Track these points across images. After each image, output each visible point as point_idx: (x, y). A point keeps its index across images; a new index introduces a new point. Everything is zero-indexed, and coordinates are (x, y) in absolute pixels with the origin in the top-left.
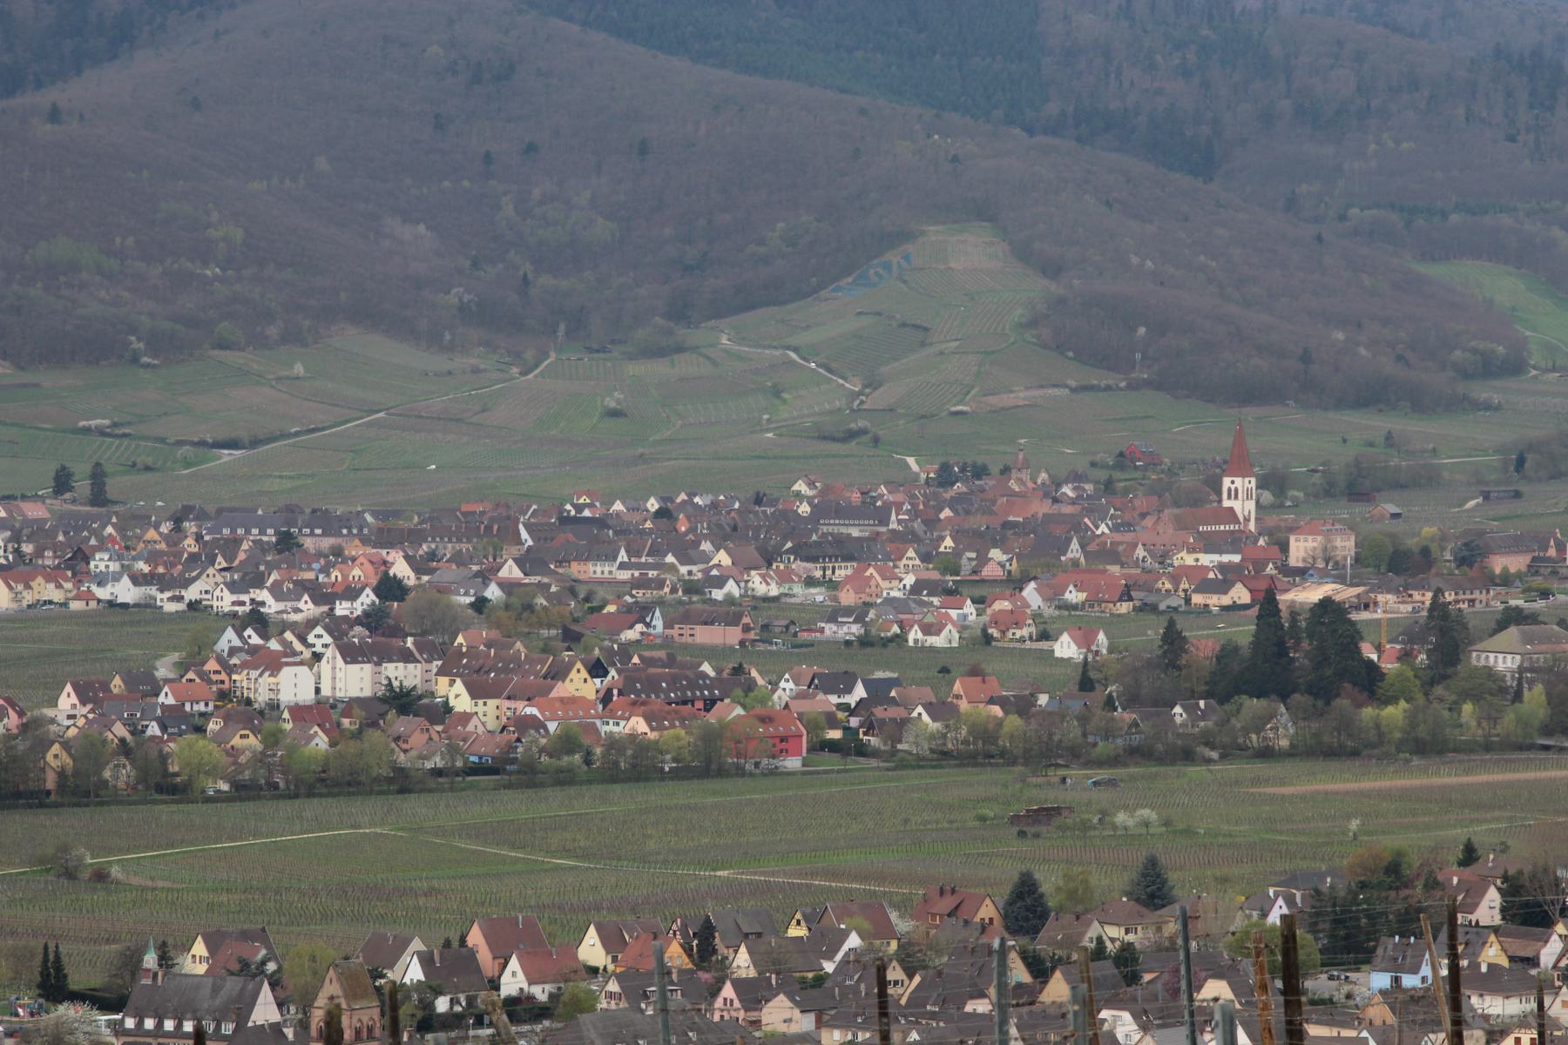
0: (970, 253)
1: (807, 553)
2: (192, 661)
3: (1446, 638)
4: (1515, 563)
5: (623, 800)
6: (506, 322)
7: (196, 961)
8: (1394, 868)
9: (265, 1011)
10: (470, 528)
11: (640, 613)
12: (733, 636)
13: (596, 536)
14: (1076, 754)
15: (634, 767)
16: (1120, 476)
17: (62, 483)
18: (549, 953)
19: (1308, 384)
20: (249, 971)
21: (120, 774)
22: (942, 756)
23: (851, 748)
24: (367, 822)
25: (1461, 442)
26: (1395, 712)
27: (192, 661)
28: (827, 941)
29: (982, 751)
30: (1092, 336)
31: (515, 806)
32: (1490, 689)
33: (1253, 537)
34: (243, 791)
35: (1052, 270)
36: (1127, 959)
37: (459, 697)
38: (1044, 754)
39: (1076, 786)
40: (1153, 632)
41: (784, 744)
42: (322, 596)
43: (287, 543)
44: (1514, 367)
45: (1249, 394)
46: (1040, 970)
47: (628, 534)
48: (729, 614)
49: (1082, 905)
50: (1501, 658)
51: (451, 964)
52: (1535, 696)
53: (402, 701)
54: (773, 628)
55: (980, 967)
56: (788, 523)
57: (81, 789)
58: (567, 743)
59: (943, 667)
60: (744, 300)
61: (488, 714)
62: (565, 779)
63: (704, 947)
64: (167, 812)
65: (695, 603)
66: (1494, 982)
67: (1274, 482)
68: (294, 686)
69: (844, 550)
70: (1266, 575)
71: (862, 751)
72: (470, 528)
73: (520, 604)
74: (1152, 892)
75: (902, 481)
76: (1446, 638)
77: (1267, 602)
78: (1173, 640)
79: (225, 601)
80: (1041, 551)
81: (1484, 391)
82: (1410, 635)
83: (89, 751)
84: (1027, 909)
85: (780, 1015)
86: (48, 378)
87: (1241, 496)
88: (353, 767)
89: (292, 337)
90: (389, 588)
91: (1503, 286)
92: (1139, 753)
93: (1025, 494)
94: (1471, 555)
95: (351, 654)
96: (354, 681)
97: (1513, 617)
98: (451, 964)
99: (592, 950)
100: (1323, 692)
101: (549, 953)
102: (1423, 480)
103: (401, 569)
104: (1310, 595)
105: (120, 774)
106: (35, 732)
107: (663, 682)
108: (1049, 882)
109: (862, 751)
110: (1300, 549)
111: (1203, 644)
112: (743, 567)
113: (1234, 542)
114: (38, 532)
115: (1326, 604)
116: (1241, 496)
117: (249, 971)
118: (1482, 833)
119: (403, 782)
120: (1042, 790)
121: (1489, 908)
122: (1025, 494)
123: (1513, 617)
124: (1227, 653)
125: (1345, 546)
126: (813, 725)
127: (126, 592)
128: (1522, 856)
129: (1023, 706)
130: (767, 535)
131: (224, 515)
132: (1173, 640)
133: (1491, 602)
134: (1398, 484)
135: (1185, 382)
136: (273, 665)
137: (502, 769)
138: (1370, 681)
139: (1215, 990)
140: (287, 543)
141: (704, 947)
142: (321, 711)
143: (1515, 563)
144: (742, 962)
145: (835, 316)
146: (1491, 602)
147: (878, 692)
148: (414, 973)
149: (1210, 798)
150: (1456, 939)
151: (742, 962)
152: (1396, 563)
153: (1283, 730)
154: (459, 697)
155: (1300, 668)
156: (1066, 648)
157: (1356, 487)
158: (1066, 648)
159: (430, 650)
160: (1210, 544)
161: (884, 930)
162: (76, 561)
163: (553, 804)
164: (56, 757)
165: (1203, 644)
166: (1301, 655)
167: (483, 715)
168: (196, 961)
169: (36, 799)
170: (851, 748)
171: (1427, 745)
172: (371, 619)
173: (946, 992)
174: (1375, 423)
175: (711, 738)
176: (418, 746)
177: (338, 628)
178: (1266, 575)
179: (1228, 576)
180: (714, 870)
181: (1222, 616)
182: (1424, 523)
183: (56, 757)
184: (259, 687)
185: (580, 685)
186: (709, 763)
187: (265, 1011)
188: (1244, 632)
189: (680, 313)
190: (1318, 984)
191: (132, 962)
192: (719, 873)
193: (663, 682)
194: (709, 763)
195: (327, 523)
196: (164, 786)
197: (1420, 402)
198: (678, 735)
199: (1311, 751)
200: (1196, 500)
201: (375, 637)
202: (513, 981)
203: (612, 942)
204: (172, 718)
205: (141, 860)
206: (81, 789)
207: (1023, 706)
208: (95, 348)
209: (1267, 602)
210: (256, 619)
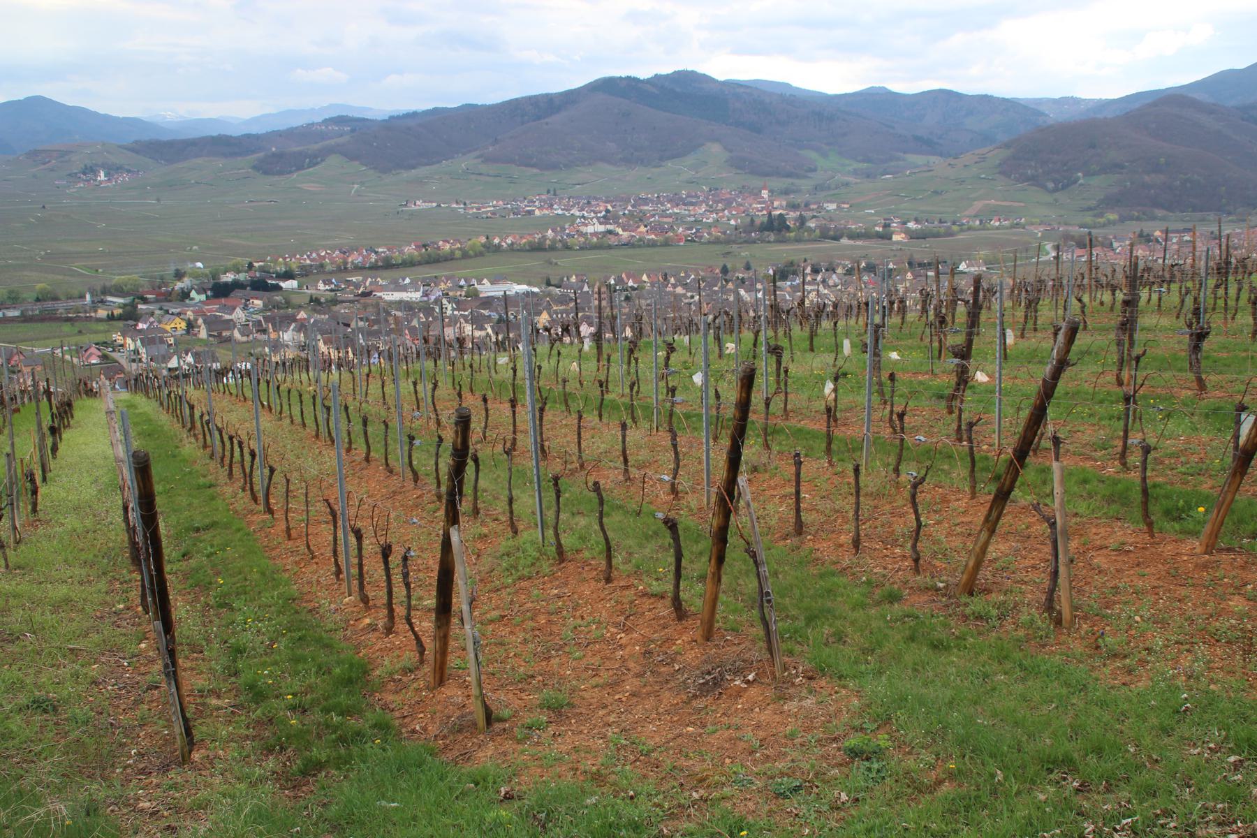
0: (715, 148)
1: (685, 204)
2: (572, 225)
3: (802, 221)
4: (815, 207)
5: (650, 250)
6: (629, 161)
7: (573, 279)
8: (792, 264)
9: (586, 288)
10: (622, 200)
11: (654, 216)
12: (670, 220)
13: (646, 201)
14: (734, 242)
15: (652, 244)
16: (742, 190)
17: (548, 192)
18: (636, 277)
19: (777, 173)
20: (583, 281)
21: (559, 245)
22: (709, 242)
23: (692, 241)
24: (603, 255)
25: (805, 184)
26: (792, 234)
27: (572, 225)
28: (688, 276)
29: (717, 241)
30: (738, 164)
31: (631, 251)
32: (810, 230)
33: (767, 201)
34: (581, 248)
35: (731, 151)
36: (743, 281)
37: (620, 231)
38: (728, 242)
39: (734, 247)
40: (748, 219)
41: (680, 240)
42: (595, 213)
43: (589, 203)
44: (814, 170)
45: (767, 175)
46: (727, 281)
47: (652, 201)
48: (670, 216)
49: (735, 270)
50: (812, 224)
51: (619, 280)
52: (818, 231)
53: (610, 232)
54: (678, 219)
55: (716, 280)
56: (682, 199)
57: (553, 248)
58: (640, 240)
59: (710, 226)
60: (673, 157)
61: (625, 235)
62: (640, 246)
63: (666, 277)
64: (568, 252)
65: (664, 214)
66: (809, 283)
67: (771, 191)
68: (590, 229)
69: (692, 204)
70: (769, 208)
71: (319, 766)
72: (622, 200)
73: (631, 214)
74: (748, 268)
75: (703, 191)
76: (802, 221)
77: (770, 214)
78: (752, 221)
79: (577, 213)
80: (728, 204)
81: (810, 174)
82: (796, 220)
83: (554, 241)
84: (725, 270)
85: (680, 290)
86: (546, 173)
87: (765, 194)
88: (601, 244)
89: (590, 164)
90: (607, 211)
91: (813, 155)
92: (746, 242)
93: (725, 193)
94: (807, 205)
95: (601, 223)
96: (601, 228)
97: (814, 217)
98: (619, 280)
99: (645, 278)
100: (780, 231)
101: (636, 277)
102: (798, 191)
103: (610, 208)
104: (778, 212)
105: (559, 245)
106: (544, 238)
107: (658, 229)
108: (729, 266)
109: (319, 766)
110: (776, 204)
111: (758, 222)
112: (673, 207)
113: (764, 202)
114: (544, 201)
115: (781, 215)
116: (765, 194)
117: (583, 281)
118: (808, 256)
119: (610, 247)
120: (727, 248)
121: (808, 270)
122: (725, 193)
123: (814, 217)
124: (762, 223)
125: (784, 203)
126: (686, 236)
127: (560, 212)
128: (815, 261)
129: (724, 233)
130: (677, 201)
131: (578, 197)
132: (752, 221)
133: (810, 214)
134: (793, 192)
135: (756, 172)
136: (586, 225)
137: (628, 245)
138: (788, 228)
139: (759, 286)
140: (589, 203)
141: (665, 279)
142: (595, 234)
143: (815, 207)
144: (672, 280)
145: (690, 160)
146: (810, 214)
147: (698, 230)
148: (613, 282)
149: (759, 250)
150: (804, 276)
151: (672, 280)
152: (793, 207)
153: (772, 237)
154: (620, 231)
155: (775, 226)
156: (732, 222)
157: (786, 192)
158: (732, 222)
159: (615, 223)
160: (760, 203)
161: (698, 274)
162: (551, 206)
163: (637, 251)
164: (548, 242)
165: (758, 222)
166: (775, 224)
167: (625, 235)
168: (573, 279)
169: (544, 250)
170: (692, 241)
171: (798, 240)
172: (604, 217)
173: (710, 285)
174: (790, 180)
175: (667, 239)
176: (612, 240)
177: (598, 218)
178: (769, 208)
179: (763, 209)
180: (527, 294)
181: (761, 217)
182: (799, 200)
183: (548, 242)
184: (584, 229)
185: (642, 229)
186: (666, 244)
187: (586, 288)
188: (765, 219)
189: (661, 159)
190: (778, 284)
191: (562, 280)
192: (523, 288)
193: (658, 229)
194: (666, 244)
195: (597, 199)
196: (567, 247)
197: (798, 176)
198: (661, 238)
199: (777, 241)
200: (757, 194)
201: (605, 220)
202: (631, 283)
203: (648, 276)
204: (568, 235)
205: (564, 261)
206: (553, 248)
207: (724, 233)
208: (554, 167)
209: (770, 214)
210: (583, 217)
